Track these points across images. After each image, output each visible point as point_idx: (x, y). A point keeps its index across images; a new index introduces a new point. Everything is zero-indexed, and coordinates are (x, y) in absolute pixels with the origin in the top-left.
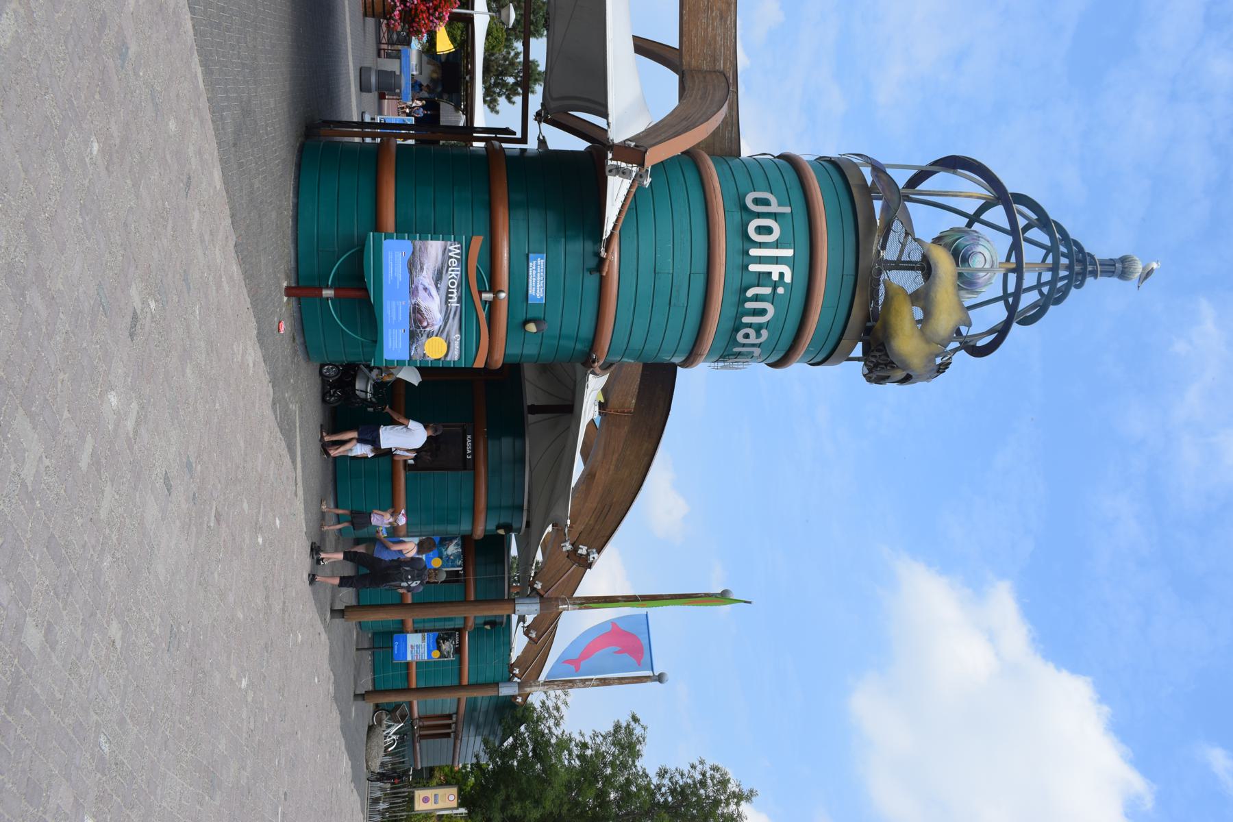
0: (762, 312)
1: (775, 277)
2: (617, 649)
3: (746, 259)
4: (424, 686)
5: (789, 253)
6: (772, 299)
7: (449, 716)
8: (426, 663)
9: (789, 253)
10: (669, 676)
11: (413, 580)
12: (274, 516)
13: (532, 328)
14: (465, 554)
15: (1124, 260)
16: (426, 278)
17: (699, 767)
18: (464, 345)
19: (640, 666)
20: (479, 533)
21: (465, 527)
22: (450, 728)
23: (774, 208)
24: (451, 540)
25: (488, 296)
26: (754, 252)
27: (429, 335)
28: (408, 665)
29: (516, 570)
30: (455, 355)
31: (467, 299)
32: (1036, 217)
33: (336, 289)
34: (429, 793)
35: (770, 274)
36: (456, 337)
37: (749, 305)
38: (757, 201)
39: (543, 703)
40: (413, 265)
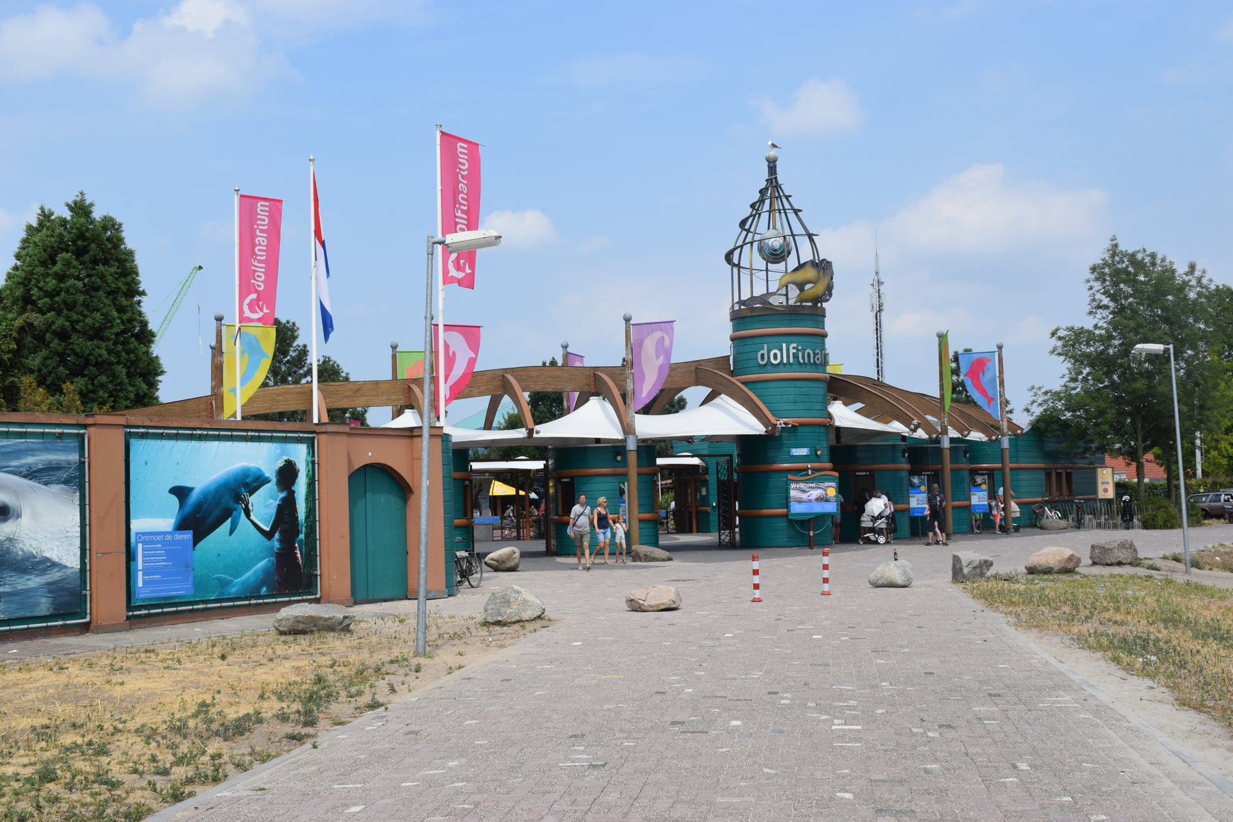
0: (809, 354)
1: (795, 351)
2: (981, 373)
3: (788, 363)
5: (784, 345)
7: (1048, 475)
9: (784, 345)
10: (999, 342)
11: (936, 499)
13: (819, 453)
14: (919, 473)
16: (804, 496)
17: (1092, 283)
18: (829, 480)
19: (992, 360)
20: (907, 466)
21: (905, 474)
22: (1061, 474)
23: (765, 352)
24: (911, 481)
25: (810, 472)
26: (785, 361)
27: (826, 494)
29: (959, 396)
30: (834, 484)
33: (810, 530)
34: (1100, 488)
35: (793, 353)
36: (826, 484)
37: (806, 361)
39: (1040, 404)
40: (800, 501)
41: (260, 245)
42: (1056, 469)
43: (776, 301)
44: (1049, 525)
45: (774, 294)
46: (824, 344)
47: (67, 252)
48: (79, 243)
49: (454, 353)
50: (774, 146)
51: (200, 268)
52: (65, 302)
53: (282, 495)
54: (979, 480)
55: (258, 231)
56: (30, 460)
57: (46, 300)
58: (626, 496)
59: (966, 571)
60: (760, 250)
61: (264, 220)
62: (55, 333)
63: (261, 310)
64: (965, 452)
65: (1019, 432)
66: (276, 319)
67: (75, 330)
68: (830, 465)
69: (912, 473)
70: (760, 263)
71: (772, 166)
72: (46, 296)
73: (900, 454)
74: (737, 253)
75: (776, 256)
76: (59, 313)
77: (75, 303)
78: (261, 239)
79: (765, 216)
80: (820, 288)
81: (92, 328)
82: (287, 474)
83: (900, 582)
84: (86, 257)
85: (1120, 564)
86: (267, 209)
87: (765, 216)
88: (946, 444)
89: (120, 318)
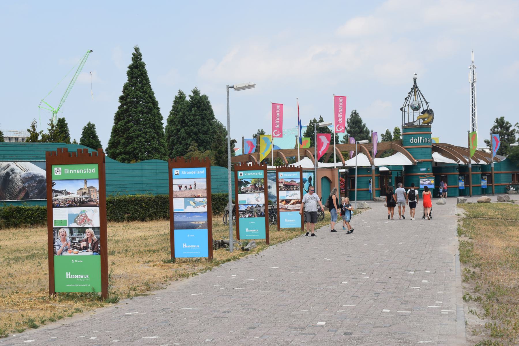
0: (426, 140)
4: (205, 180)
5: (418, 137)
6: (424, 139)
8: (465, 182)
9: (418, 137)
13: (429, 170)
15: (414, 79)
16: (424, 183)
18: (432, 178)
20: (458, 173)
21: (457, 176)
23: (412, 139)
24: (459, 178)
26: (419, 142)
28: (488, 186)
30: (433, 179)
31: (426, 178)
36: (431, 179)
38: (412, 141)
42: (516, 173)
43: (415, 124)
44: (510, 192)
45: (415, 122)
46: (431, 136)
47: (195, 107)
48: (198, 104)
49: (323, 142)
50: (416, 74)
51: (91, 51)
52: (196, 123)
53: (309, 184)
54: (484, 177)
56: (273, 177)
57: (190, 123)
58: (371, 183)
59: (460, 201)
60: (411, 107)
62: (193, 133)
64: (480, 168)
65: (499, 161)
66: (310, 147)
67: (199, 132)
68: (432, 174)
69: (460, 175)
70: (411, 110)
71: (415, 82)
72: (190, 121)
73: (456, 169)
74: (404, 108)
75: (416, 109)
76: (194, 127)
77: (199, 123)
79: (413, 97)
80: (430, 120)
81: (204, 131)
82: (310, 179)
83: (443, 203)
84: (200, 109)
85: (504, 201)
87: (413, 97)
88: (470, 166)
89: (211, 128)
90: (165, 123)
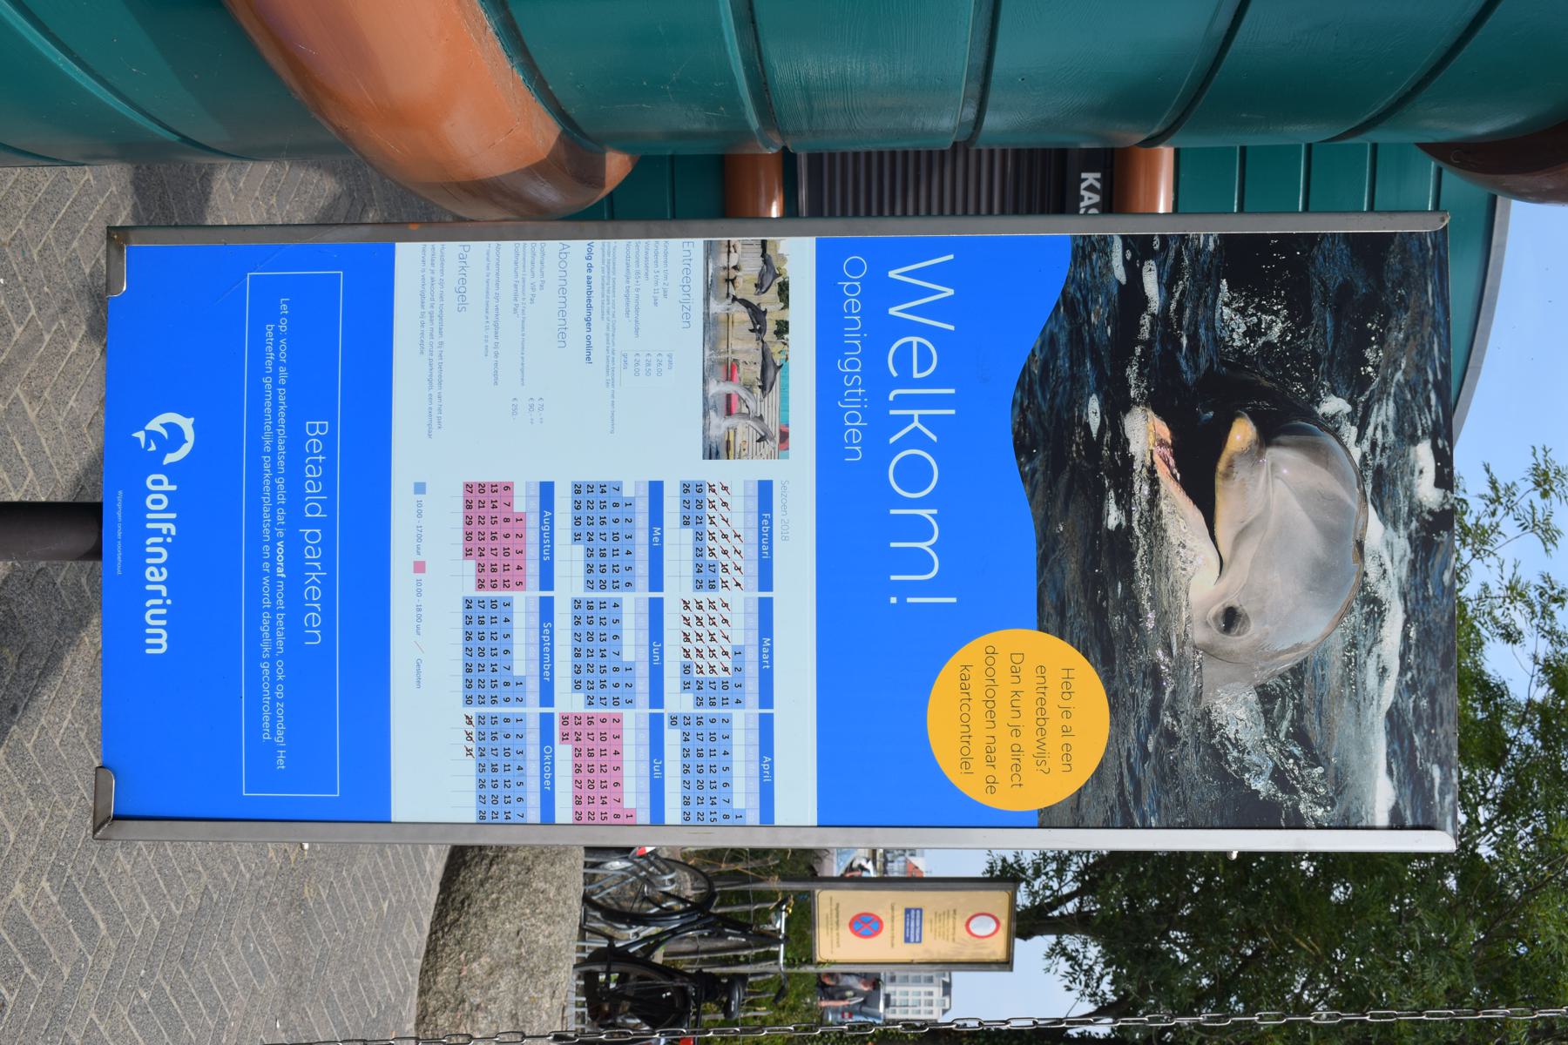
1: (165, 532)
5: (173, 516)
9: (173, 516)
12: (1116, 408)
32: (1123, 280)
35: (161, 530)
41: (158, 566)
55: (164, 594)
61: (154, 617)
63: (151, 435)
78: (157, 578)
86: (149, 641)
90: (1094, 436)
